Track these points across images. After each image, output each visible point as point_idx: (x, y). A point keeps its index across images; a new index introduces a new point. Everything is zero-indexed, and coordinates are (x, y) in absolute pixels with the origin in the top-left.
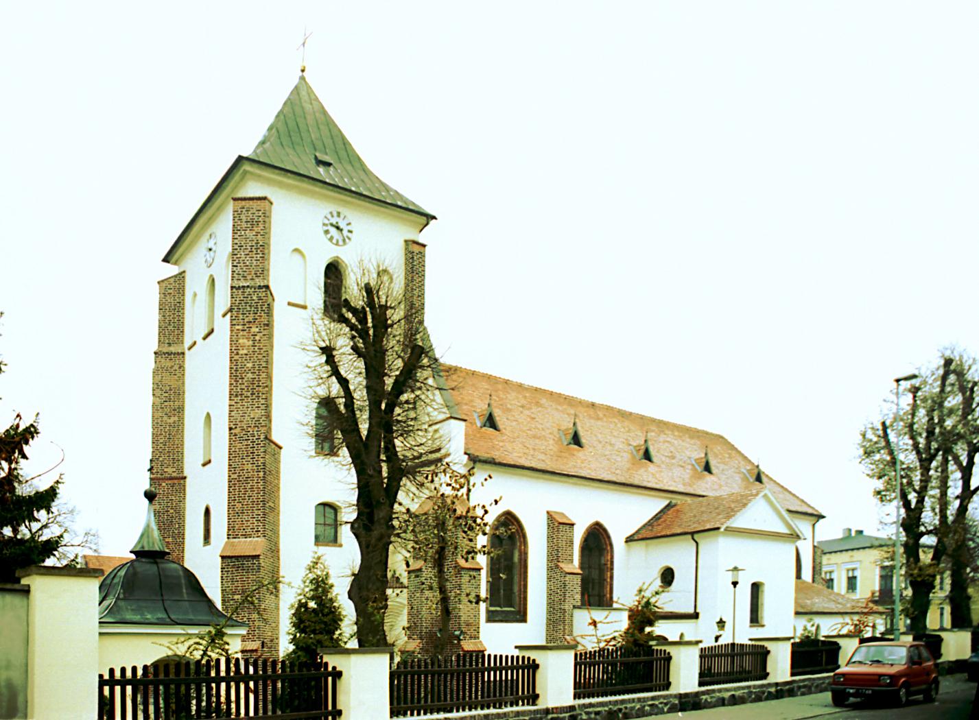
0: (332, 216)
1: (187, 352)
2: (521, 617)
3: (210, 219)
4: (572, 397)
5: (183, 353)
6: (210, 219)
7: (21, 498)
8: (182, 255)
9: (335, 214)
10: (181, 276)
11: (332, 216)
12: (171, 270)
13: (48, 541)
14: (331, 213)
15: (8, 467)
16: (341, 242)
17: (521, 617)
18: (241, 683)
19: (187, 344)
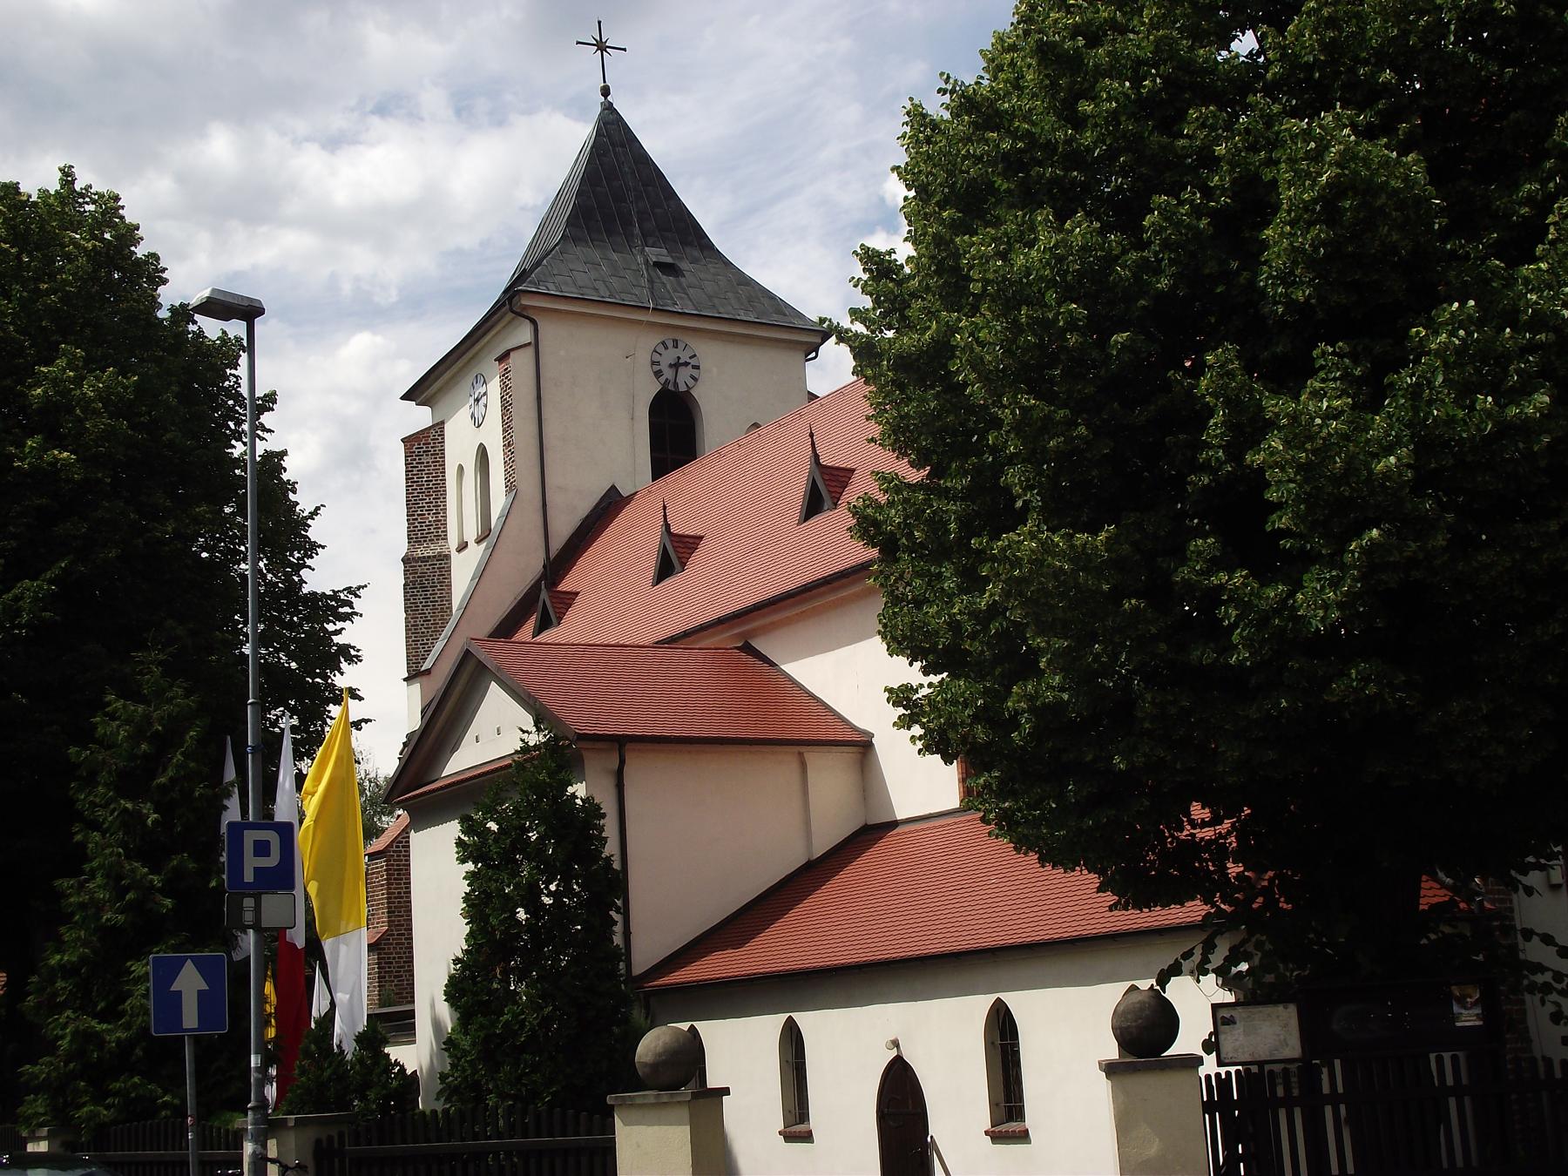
0: (666, 348)
1: (454, 554)
2: (256, 842)
3: (469, 361)
4: (405, 744)
5: (448, 557)
6: (472, 358)
7: (1140, 261)
8: (440, 390)
9: (670, 344)
10: (439, 427)
11: (666, 348)
12: (420, 417)
13: (107, 702)
14: (663, 343)
15: (1524, 882)
16: (695, 373)
17: (256, 842)
18: (1353, 1172)
19: (453, 542)
